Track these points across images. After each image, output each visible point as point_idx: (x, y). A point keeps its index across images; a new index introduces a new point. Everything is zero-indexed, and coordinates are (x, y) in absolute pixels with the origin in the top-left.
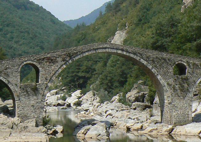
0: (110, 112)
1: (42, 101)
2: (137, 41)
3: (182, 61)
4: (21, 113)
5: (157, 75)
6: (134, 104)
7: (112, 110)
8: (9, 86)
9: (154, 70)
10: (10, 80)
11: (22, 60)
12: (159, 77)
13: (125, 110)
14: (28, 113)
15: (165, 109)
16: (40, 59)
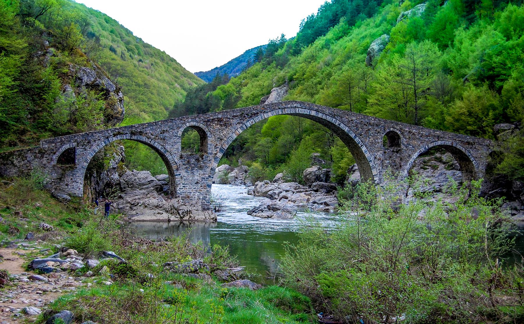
0: (284, 194)
1: (209, 176)
2: (20, 200)
3: (395, 128)
4: (181, 192)
5: (362, 146)
6: (314, 184)
7: (287, 191)
8: (167, 156)
9: (357, 140)
10: (168, 147)
11: (184, 120)
12: (364, 149)
13: (303, 192)
14: (191, 193)
15: (177, 179)
16: (208, 121)
